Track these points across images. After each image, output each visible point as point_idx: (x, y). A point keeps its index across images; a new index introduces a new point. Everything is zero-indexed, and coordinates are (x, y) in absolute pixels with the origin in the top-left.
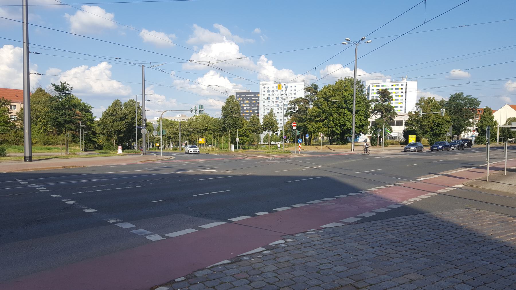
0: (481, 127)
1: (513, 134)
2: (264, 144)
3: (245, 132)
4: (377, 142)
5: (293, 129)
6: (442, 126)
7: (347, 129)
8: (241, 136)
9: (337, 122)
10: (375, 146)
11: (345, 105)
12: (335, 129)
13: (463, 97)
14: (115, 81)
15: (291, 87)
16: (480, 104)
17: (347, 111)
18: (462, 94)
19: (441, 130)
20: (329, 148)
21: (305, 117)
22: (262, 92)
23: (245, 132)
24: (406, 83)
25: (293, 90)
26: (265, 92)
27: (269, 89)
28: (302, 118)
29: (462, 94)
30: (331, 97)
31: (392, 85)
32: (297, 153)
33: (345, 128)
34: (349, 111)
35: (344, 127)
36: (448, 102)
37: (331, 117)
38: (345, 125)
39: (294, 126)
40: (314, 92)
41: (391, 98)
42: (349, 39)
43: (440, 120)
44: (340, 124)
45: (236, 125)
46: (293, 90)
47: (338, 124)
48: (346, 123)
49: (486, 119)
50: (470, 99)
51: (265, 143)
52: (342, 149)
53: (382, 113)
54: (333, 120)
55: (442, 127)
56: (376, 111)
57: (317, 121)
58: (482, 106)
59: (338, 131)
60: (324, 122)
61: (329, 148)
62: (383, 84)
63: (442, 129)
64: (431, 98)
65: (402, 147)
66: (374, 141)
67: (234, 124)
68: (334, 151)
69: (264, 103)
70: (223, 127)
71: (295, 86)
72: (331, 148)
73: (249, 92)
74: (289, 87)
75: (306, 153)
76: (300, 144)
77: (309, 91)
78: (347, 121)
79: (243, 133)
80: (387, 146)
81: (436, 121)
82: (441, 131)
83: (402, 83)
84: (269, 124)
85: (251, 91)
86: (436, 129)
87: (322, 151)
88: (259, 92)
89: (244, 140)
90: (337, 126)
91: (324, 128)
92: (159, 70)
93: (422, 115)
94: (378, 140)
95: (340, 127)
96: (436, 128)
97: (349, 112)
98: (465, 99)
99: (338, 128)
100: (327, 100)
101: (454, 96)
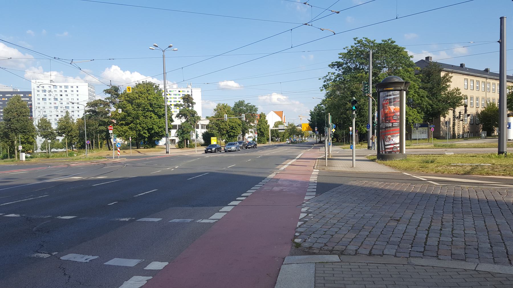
0: (260, 129)
1: (280, 135)
2: (42, 151)
3: (28, 138)
4: (184, 145)
5: (110, 132)
6: (235, 129)
7: (155, 132)
8: (22, 143)
9: (145, 126)
10: (183, 148)
11: (151, 109)
12: (142, 132)
13: (245, 104)
14: (72, 78)
15: (72, 87)
16: (257, 110)
17: (154, 115)
18: (244, 101)
19: (234, 133)
20: (139, 152)
21: (108, 120)
22: (36, 91)
23: (28, 138)
24: (191, 89)
25: (75, 92)
26: (39, 91)
27: (45, 88)
28: (105, 121)
29: (244, 101)
30: (134, 100)
31: (179, 91)
32: (115, 158)
33: (153, 132)
34: (155, 115)
35: (152, 130)
36: (233, 109)
37: (138, 120)
38: (152, 129)
39: (111, 129)
40: (115, 94)
41: (193, 103)
42: (157, 45)
43: (233, 124)
44: (148, 127)
45: (25, 129)
46: (75, 92)
47: (146, 127)
48: (154, 127)
49: (262, 123)
50: (250, 106)
51: (44, 151)
52: (152, 152)
53: (186, 118)
54: (139, 123)
55: (235, 130)
56: (181, 115)
57: (122, 124)
58: (259, 112)
59: (146, 134)
60: (130, 125)
61: (139, 152)
62: (170, 90)
63: (236, 132)
64: (225, 105)
65: (204, 148)
66: (182, 143)
67: (22, 128)
68: (145, 154)
69: (61, 105)
70: (4, 133)
71: (77, 87)
72: (141, 152)
73: (16, 91)
74: (70, 87)
75: (125, 158)
76: (119, 148)
77: (109, 93)
78: (154, 124)
79: (25, 140)
80: (193, 148)
81: (231, 124)
82: (235, 134)
83: (188, 90)
84: (65, 128)
85: (19, 90)
86: (231, 132)
87: (131, 155)
88: (31, 92)
89: (27, 148)
90: (144, 130)
91: (130, 132)
92: (77, 67)
93: (227, 119)
94: (185, 142)
95: (148, 130)
96: (230, 130)
97: (155, 116)
98: (247, 105)
99: (146, 131)
100: (131, 102)
101: (238, 103)
